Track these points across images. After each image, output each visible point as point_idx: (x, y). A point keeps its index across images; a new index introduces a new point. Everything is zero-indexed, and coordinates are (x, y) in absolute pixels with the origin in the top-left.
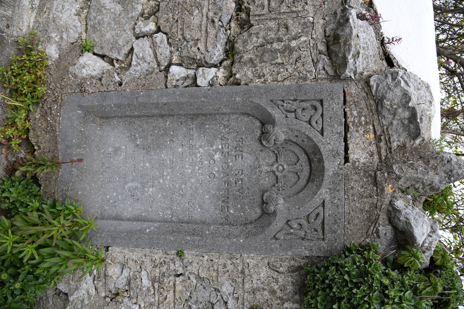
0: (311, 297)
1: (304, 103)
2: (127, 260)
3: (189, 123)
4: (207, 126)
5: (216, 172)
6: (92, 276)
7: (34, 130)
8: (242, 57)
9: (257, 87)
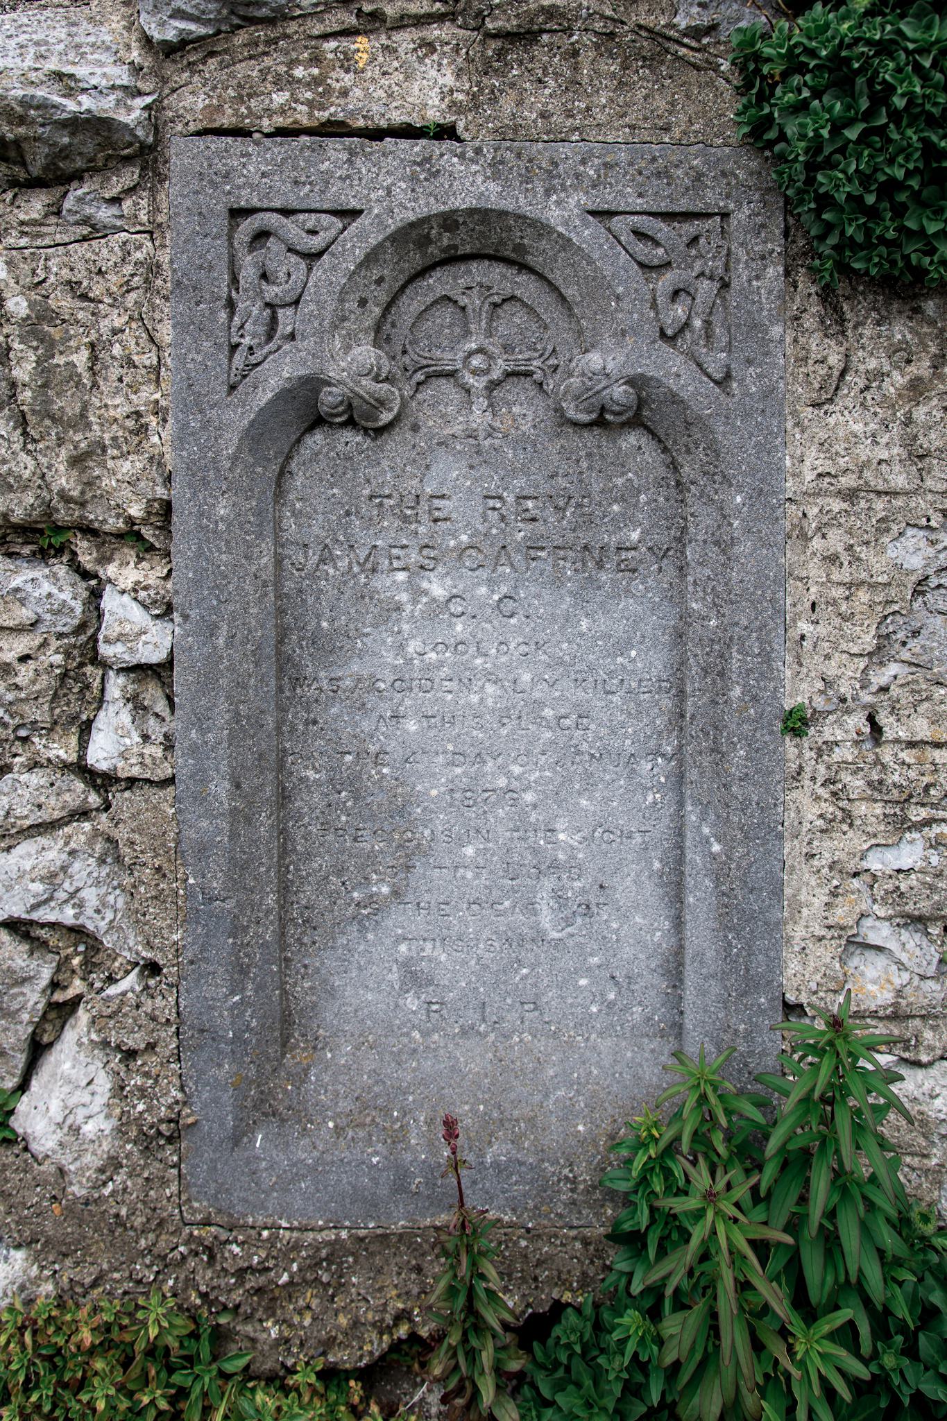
0: (926, 253)
1: (243, 274)
2: (829, 927)
3: (311, 692)
4: (325, 624)
5: (493, 591)
6: (904, 1071)
7: (329, 1344)
8: (64, 497)
9: (180, 440)
